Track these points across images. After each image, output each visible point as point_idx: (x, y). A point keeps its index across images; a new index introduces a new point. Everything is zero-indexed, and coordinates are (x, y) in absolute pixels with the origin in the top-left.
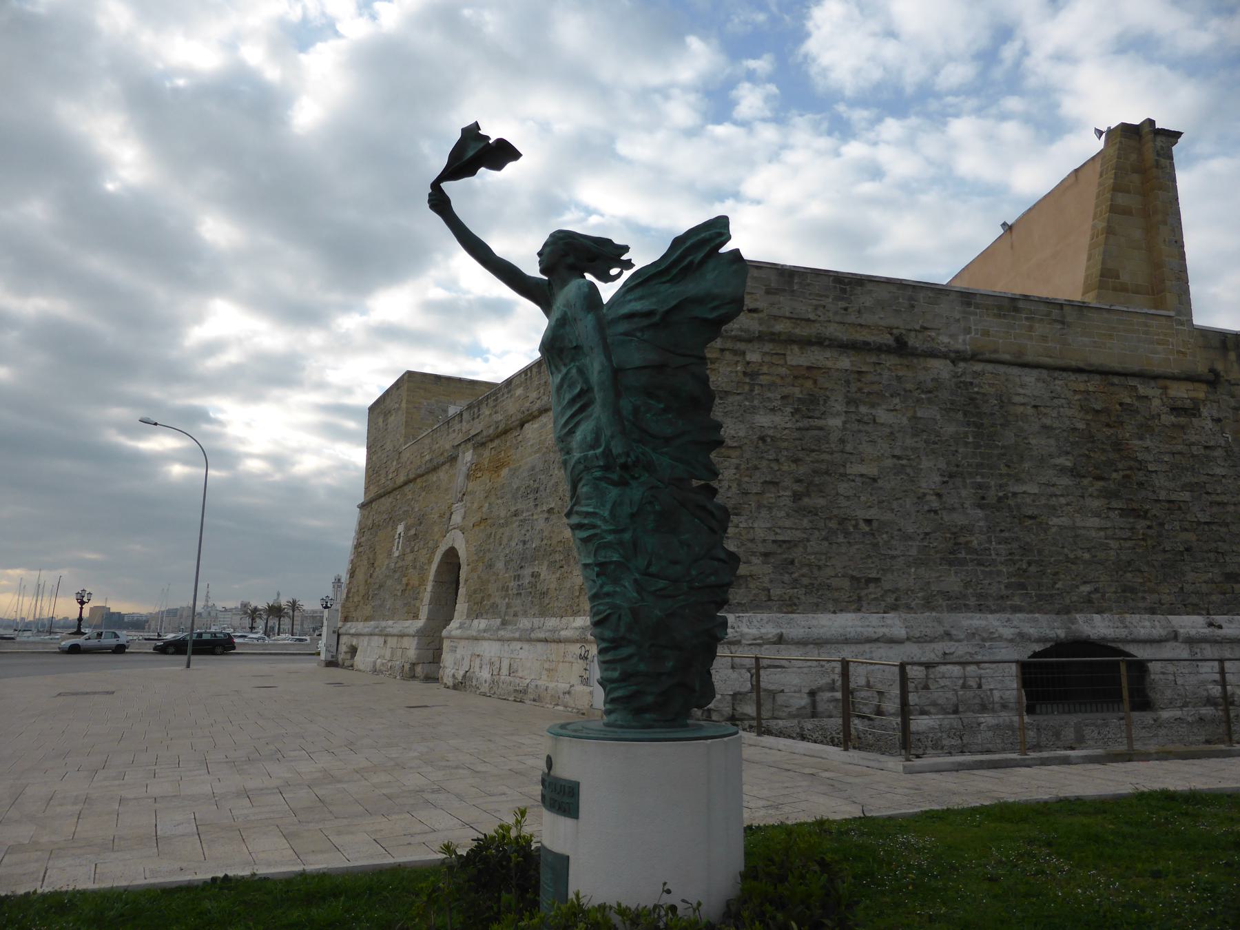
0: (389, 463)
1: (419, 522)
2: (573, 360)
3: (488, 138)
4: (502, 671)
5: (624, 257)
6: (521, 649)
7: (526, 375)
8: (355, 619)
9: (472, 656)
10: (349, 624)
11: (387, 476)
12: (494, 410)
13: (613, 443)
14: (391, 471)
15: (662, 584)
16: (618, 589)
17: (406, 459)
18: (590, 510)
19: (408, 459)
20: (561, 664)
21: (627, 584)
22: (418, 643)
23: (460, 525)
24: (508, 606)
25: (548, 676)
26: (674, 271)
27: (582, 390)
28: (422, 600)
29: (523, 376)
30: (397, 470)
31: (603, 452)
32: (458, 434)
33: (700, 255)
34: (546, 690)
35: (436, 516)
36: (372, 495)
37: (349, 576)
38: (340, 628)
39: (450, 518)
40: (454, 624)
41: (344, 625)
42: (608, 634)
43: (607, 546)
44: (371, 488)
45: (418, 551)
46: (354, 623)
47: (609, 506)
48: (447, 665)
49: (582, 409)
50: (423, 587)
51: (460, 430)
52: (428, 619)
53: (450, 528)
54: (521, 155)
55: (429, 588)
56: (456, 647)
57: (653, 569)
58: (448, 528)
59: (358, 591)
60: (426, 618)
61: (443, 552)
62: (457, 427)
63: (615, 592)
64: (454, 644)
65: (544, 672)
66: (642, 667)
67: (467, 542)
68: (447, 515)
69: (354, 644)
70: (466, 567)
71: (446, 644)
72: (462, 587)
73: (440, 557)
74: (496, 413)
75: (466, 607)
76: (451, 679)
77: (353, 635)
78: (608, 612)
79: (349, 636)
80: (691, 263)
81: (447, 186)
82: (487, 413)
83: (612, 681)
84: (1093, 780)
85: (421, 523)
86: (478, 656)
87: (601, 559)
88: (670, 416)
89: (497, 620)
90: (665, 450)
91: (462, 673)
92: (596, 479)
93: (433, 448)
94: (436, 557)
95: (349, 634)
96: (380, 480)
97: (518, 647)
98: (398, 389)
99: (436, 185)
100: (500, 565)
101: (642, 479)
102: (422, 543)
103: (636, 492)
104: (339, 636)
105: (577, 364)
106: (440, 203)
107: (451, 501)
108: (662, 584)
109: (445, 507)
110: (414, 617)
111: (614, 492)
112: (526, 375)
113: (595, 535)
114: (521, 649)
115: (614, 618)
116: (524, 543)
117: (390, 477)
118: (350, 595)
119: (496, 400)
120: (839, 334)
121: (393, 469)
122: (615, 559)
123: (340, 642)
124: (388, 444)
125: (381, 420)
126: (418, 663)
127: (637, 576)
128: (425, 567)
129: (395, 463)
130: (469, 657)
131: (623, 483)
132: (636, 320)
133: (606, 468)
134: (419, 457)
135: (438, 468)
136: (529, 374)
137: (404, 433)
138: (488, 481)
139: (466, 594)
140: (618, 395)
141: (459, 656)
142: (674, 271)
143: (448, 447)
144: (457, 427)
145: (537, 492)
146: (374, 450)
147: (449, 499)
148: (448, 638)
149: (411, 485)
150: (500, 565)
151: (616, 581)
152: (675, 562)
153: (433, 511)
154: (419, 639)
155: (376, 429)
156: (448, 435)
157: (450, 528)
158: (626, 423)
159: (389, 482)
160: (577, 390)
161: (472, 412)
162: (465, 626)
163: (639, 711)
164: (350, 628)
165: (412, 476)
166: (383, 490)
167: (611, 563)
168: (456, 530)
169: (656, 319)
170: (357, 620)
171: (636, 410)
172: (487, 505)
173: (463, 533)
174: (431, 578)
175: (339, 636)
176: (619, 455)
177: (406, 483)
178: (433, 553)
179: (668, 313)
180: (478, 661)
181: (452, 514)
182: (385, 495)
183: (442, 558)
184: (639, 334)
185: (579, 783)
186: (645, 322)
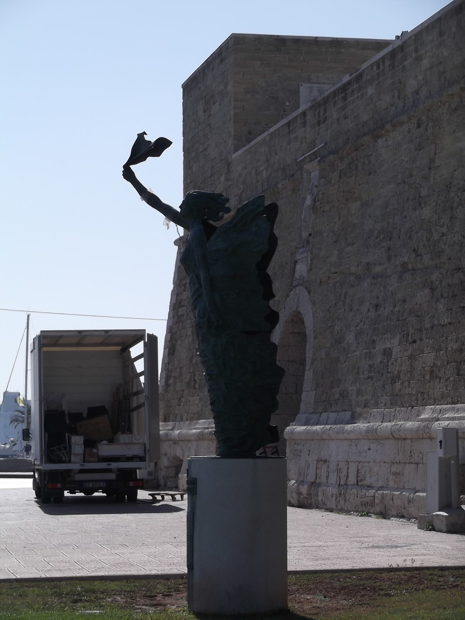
3: (150, 142)
4: (349, 479)
5: (227, 205)
6: (369, 449)
7: (378, 67)
8: (178, 417)
9: (318, 461)
12: (343, 113)
20: (407, 465)
24: (359, 393)
25: (395, 482)
29: (375, 68)
32: (302, 143)
34: (392, 499)
53: (295, 283)
54: (171, 143)
56: (301, 452)
58: (292, 283)
59: (181, 374)
65: (391, 477)
67: (314, 304)
69: (178, 454)
74: (345, 117)
76: (295, 495)
81: (133, 167)
82: (335, 116)
84: (389, 467)
86: (325, 461)
89: (347, 412)
97: (366, 448)
98: (222, 61)
100: (350, 338)
106: (128, 175)
112: (378, 67)
114: (369, 449)
116: (377, 306)
118: (171, 381)
119: (345, 99)
120: (189, 333)
129: (223, 178)
130: (315, 462)
136: (381, 67)
137: (232, 133)
138: (337, 219)
145: (390, 239)
150: (350, 338)
155: (194, 121)
161: (317, 112)
168: (301, 287)
170: (182, 420)
172: (336, 252)
180: (324, 468)
181: (296, 262)
185: (197, 478)
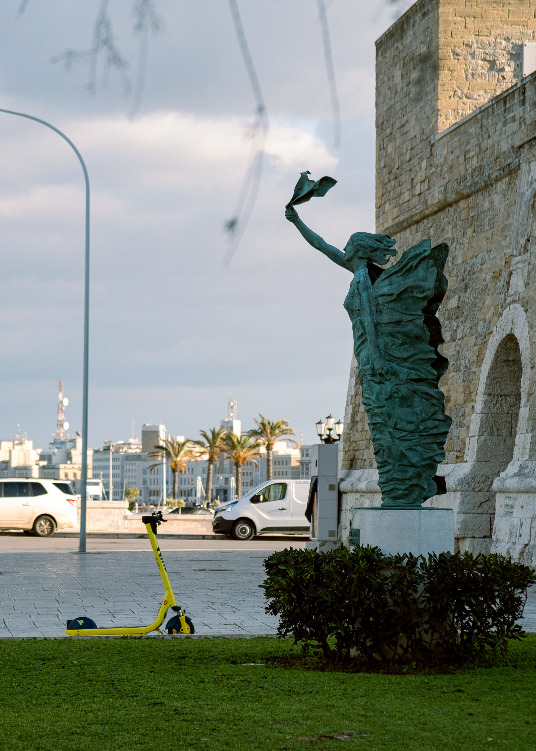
0: (415, 161)
1: (463, 284)
2: (358, 316)
8: (367, 463)
10: (357, 473)
11: (413, 187)
13: (375, 363)
14: (419, 178)
15: (404, 434)
16: (382, 437)
17: (442, 160)
18: (368, 396)
19: (446, 159)
21: (386, 434)
22: (462, 503)
23: (521, 296)
26: (404, 270)
27: (362, 333)
28: (468, 427)
30: (428, 179)
31: (371, 367)
33: (416, 262)
35: (489, 277)
36: (389, 223)
37: (354, 379)
38: (342, 480)
39: (508, 283)
40: (512, 468)
41: (348, 475)
42: (380, 460)
43: (375, 415)
44: (387, 207)
45: (462, 338)
46: (366, 471)
47: (375, 395)
48: (500, 537)
49: (363, 342)
50: (470, 405)
51: (523, 119)
52: (478, 460)
53: (509, 300)
55: (479, 406)
56: (512, 507)
57: (398, 426)
58: (505, 300)
60: (474, 458)
61: (497, 343)
62: (518, 112)
63: (381, 438)
64: (510, 502)
66: (396, 476)
68: (504, 277)
70: (529, 370)
71: (500, 501)
72: (525, 406)
73: (494, 351)
75: (529, 439)
77: (363, 493)
78: (379, 448)
79: (358, 495)
80: (412, 266)
83: (383, 483)
85: (466, 287)
87: (374, 421)
88: (406, 346)
90: (403, 364)
91: (519, 548)
92: (369, 380)
93: (483, 146)
94: (488, 351)
95: (357, 492)
96: (401, 194)
99: (289, 207)
101: (392, 380)
102: (468, 325)
103: (388, 387)
104: (340, 494)
105: (360, 318)
107: (509, 251)
108: (404, 434)
109: (501, 260)
110: (457, 457)
111: (377, 387)
113: (370, 409)
115: (381, 451)
117: (418, 190)
118: (358, 418)
121: (421, 176)
122: (380, 421)
123: (344, 507)
124: (412, 122)
125: (398, 73)
126: (464, 538)
127: (391, 430)
128: (473, 369)
129: (424, 164)
130: (529, 521)
131: (380, 383)
132: (385, 297)
133: (373, 375)
134: (461, 159)
135: (492, 185)
139: (529, 417)
140: (377, 337)
141: (516, 522)
142: (404, 270)
143: (505, 147)
144: (518, 112)
146: (388, 131)
147: (506, 247)
148: (501, 491)
149: (451, 210)
151: (381, 432)
152: (411, 423)
153: (484, 267)
154: (464, 496)
156: (505, 125)
157: (509, 300)
158: (382, 352)
159: (415, 200)
160: (360, 333)
162: (527, 471)
163: (396, 498)
164: (359, 479)
165: (451, 197)
166: (407, 215)
167: (378, 423)
169: (394, 297)
171: (386, 346)
173: (526, 311)
174: (481, 388)
175: (340, 494)
176: (378, 369)
177: (444, 207)
178: (485, 343)
179: (400, 294)
181: (510, 274)
182: (409, 226)
183: (498, 352)
184: (386, 305)
186: (390, 299)
